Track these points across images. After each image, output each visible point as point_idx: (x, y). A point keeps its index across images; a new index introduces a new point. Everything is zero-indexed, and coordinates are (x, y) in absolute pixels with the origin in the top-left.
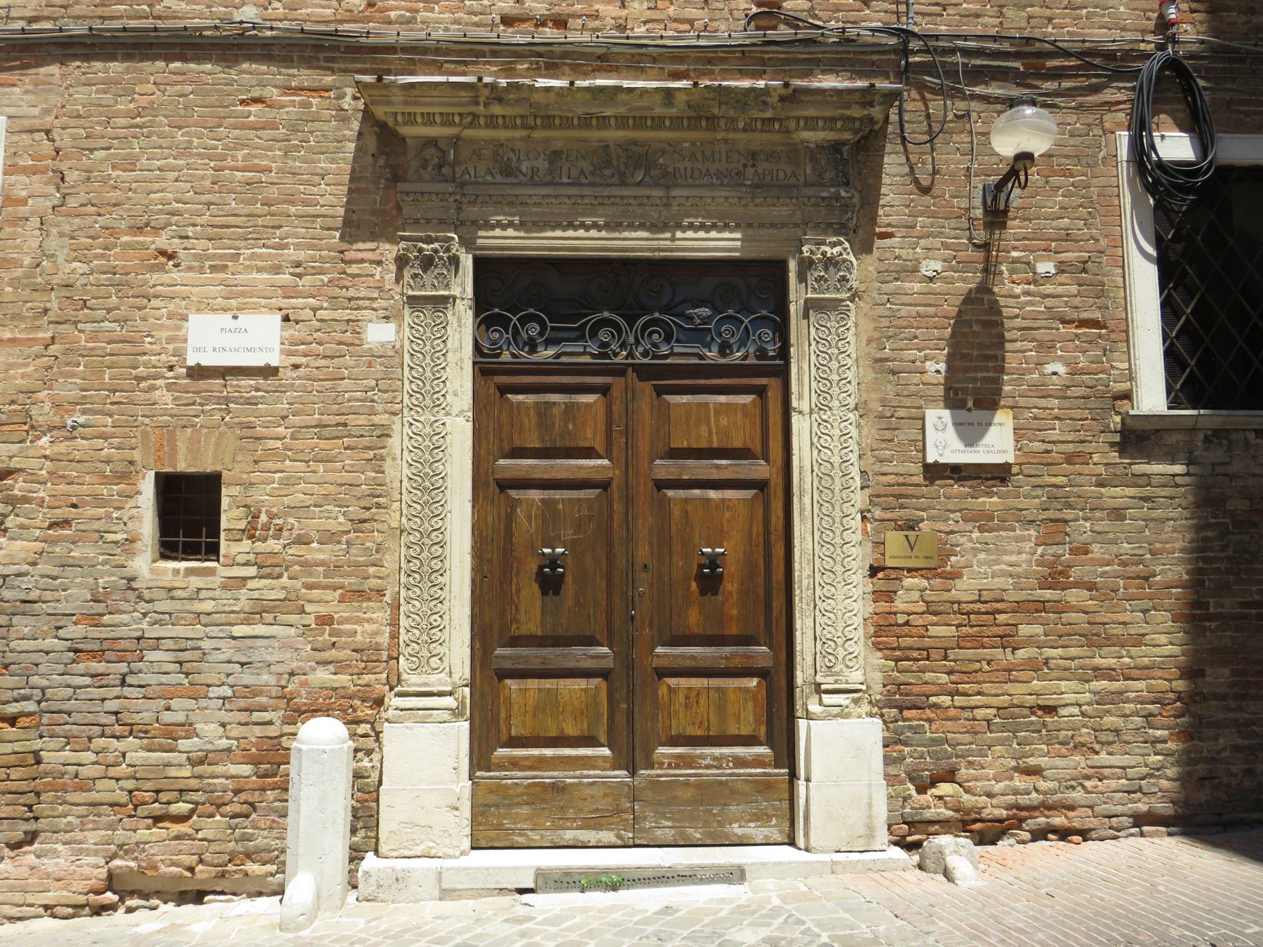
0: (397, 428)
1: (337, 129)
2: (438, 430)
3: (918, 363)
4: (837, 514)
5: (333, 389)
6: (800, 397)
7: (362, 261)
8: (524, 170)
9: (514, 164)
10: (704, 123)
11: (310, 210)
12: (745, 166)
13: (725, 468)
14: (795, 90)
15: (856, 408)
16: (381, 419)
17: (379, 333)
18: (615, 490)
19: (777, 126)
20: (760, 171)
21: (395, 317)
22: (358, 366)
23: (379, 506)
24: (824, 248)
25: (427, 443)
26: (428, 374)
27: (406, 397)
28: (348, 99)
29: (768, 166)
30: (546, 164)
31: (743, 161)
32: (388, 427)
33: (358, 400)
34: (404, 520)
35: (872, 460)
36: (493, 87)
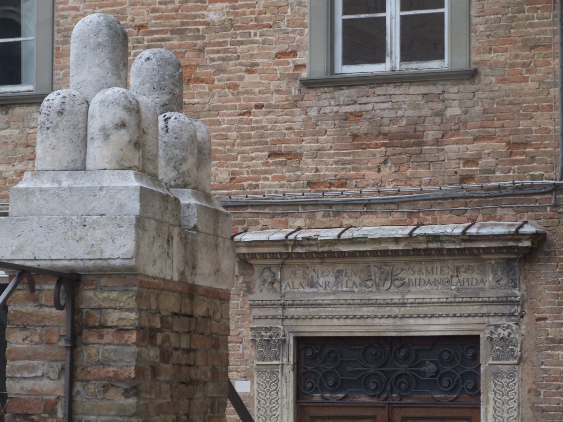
8: (321, 283)
9: (315, 280)
12: (452, 276)
26: (268, 413)
29: (466, 276)
31: (451, 273)
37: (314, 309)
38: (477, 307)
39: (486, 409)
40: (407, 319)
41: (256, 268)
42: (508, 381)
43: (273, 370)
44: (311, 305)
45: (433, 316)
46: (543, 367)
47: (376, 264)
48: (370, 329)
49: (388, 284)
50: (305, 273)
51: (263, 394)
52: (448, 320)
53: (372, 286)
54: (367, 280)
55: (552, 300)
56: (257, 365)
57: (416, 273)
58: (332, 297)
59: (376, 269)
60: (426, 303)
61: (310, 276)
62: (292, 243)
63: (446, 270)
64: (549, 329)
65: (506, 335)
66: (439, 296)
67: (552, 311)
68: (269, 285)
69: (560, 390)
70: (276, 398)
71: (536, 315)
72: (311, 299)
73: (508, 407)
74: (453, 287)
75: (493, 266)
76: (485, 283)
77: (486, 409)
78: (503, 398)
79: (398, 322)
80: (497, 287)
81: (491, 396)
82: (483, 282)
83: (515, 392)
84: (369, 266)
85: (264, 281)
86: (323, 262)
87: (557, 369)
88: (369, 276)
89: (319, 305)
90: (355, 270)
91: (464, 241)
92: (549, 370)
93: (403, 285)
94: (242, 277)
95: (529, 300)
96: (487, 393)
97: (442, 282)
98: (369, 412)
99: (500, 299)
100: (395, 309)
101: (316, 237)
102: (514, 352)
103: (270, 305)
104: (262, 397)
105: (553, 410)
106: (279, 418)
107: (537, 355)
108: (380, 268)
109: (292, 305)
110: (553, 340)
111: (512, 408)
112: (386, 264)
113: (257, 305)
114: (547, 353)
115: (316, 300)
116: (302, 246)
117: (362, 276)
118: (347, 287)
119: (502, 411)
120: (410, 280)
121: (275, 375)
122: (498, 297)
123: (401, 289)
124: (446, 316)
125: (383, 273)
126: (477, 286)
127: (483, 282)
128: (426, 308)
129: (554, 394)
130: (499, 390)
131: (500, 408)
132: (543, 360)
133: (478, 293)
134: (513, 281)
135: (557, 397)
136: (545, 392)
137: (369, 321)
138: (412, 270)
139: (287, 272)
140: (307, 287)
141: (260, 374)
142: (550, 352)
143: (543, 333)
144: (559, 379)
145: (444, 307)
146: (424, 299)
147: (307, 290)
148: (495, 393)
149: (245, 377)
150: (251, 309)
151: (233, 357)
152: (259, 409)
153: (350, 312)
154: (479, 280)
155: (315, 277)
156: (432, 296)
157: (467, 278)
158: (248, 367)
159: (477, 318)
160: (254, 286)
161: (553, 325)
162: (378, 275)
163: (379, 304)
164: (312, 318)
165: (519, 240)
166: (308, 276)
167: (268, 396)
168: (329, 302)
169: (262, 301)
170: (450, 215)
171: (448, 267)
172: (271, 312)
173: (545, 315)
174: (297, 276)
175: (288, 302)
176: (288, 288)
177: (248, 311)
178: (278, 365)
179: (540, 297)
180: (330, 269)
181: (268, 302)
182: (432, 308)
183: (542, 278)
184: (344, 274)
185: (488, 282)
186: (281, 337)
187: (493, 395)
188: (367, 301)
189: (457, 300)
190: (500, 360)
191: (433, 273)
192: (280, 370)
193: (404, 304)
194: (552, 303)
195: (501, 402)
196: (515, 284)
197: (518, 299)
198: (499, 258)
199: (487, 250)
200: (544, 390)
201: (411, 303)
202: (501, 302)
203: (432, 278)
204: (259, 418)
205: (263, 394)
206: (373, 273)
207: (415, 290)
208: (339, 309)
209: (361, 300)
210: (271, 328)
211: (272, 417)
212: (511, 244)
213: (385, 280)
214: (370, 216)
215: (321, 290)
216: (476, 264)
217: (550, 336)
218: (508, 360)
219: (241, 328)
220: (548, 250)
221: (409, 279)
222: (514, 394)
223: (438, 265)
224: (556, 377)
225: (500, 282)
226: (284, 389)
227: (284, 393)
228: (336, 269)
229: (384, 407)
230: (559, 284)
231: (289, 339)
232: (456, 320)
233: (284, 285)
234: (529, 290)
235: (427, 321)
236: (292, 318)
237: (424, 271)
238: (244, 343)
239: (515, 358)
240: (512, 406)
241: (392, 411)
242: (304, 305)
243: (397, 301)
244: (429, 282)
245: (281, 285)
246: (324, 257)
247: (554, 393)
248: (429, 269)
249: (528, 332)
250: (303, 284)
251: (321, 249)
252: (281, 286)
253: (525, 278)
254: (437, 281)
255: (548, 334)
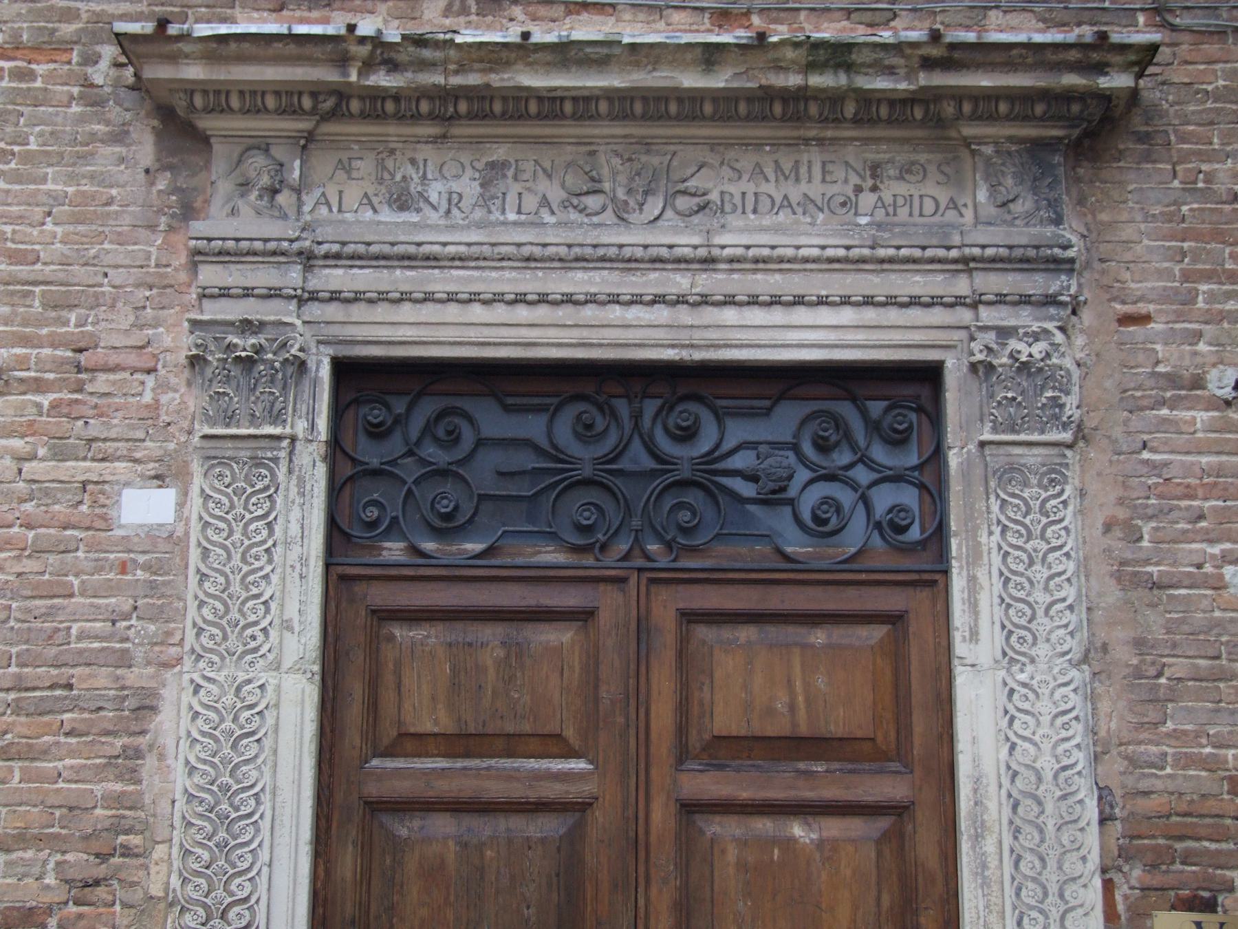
0: (168, 693)
1: (81, 119)
2: (251, 700)
3: (1208, 568)
4: (1052, 878)
5: (49, 614)
6: (974, 635)
7: (116, 368)
8: (434, 198)
9: (414, 187)
10: (778, 109)
11: (22, 270)
12: (858, 190)
13: (825, 781)
14: (953, 46)
15: (1085, 659)
16: (136, 676)
17: (145, 507)
18: (600, 818)
19: (918, 113)
20: (888, 198)
21: (176, 476)
22: (99, 570)
23: (127, 852)
24: (1013, 344)
25: (228, 724)
26: (236, 588)
27: (190, 634)
28: (104, 64)
29: (901, 188)
30: (476, 188)
31: (854, 180)
32: (154, 694)
33: (97, 638)
34: (175, 882)
35: (1121, 765)
36: (376, 41)
37: (409, 273)
38: (940, 277)
39: (972, 580)
40: (715, 310)
41: (218, 147)
42: (1044, 495)
43: (260, 454)
44: (403, 257)
45: (799, 301)
46: (1146, 455)
47: (615, 147)
48: (594, 336)
49: (654, 206)
50: (381, 165)
51: (218, 530)
52: (847, 315)
53: (604, 209)
54: (587, 193)
55: (1166, 265)
56: (205, 437)
57: (746, 177)
58: (474, 237)
59: (616, 161)
60: (781, 260)
61: (398, 178)
62: (364, 50)
63: (839, 173)
64: (1158, 347)
65: (1038, 356)
66: (822, 242)
67: (1165, 297)
68: (260, 197)
69: (1203, 524)
70: (264, 542)
71: (1118, 307)
72: (402, 238)
73: (1046, 573)
74: (863, 220)
75: (988, 161)
76: (963, 210)
77: (972, 580)
78: (1028, 546)
79: (684, 315)
80: (1005, 222)
81: (990, 541)
82: (956, 208)
83: (1066, 528)
84: (592, 153)
85: (245, 186)
86: (444, 136)
87: (1193, 464)
88: (593, 179)
89: (427, 258)
90: (547, 165)
91: (928, 64)
92: (1166, 464)
93: (702, 208)
94: (168, 174)
95: (1097, 266)
96: (973, 533)
97: (825, 206)
98: (570, 598)
99: (1018, 253)
100: (678, 277)
101: (448, 36)
102: (1062, 406)
103: (264, 253)
104: (215, 538)
105: (1186, 583)
106: (273, 605)
107: (1126, 422)
108: (630, 160)
109: (337, 256)
110: (1172, 380)
111: (1060, 574)
112: (646, 145)
113: (220, 253)
114: (1156, 416)
115: (419, 244)
116: (393, 66)
117: (569, 180)
118: (519, 212)
119: (1027, 585)
120: (727, 197)
121: (264, 472)
122: (1010, 247)
123: (696, 219)
124: (842, 303)
125: (638, 174)
126: (937, 219)
127: (956, 208)
128: (778, 277)
129: (1185, 537)
130: (1016, 522)
131: (1022, 575)
132: (1146, 437)
133: (946, 235)
134: (1049, 205)
135: (1194, 546)
136: (1156, 529)
137: (589, 312)
138: (733, 169)
139: (323, 163)
140: (386, 208)
141: (213, 466)
142: (1165, 412)
143: (1141, 357)
144: (1200, 493)
145: (836, 276)
146: (773, 247)
147: (387, 215)
148: (1005, 529)
149: (157, 477)
150: (193, 267)
151: (120, 414)
152: (203, 577)
153: (531, 282)
154: (943, 202)
155: (416, 180)
156: (803, 240)
157: (907, 194)
158: (172, 446)
159: (937, 310)
160: (207, 202)
161: (1169, 338)
162: (622, 179)
163: (629, 260)
164: (400, 300)
165: (1101, 68)
166: (393, 176)
167: (237, 536)
168: (462, 249)
169: (237, 240)
170: (845, 23)
171: (847, 163)
172: (263, 276)
173: (1143, 308)
174: (355, 174)
175: (324, 248)
176: (324, 210)
177: (183, 276)
178: (279, 438)
179: (1128, 256)
180: (465, 158)
181: (258, 245)
182: (796, 278)
183: (1131, 204)
184: (510, 173)
185: (979, 209)
186: (293, 351)
187: (996, 537)
188: (588, 251)
189: (882, 253)
190: (1018, 433)
191: (797, 180)
192: (283, 454)
193: (709, 262)
194: (1167, 274)
195: (1024, 557)
196: (1055, 212)
197: (1071, 253)
198: (1011, 139)
199: (985, 105)
200: (1154, 525)
201: (731, 261)
202: (1021, 261)
203: (795, 193)
204: (202, 604)
205: (218, 530)
206: (605, 171)
207: (741, 223)
208: (494, 274)
209: (570, 246)
210: (262, 324)
211: (250, 604)
212: (1071, 80)
213: (646, 193)
214: (596, 18)
215: (434, 217)
216: (931, 156)
217: (1161, 369)
218: (1042, 432)
219: (155, 327)
220: (1144, 129)
221: (722, 193)
222: (1063, 533)
223: (814, 156)
224: (1188, 486)
225: (1011, 206)
226: (295, 514)
227: (294, 529)
228: (484, 160)
229: (623, 580)
230: (1183, 220)
231: (319, 363)
232: (870, 315)
233: (309, 201)
234: (1094, 235)
235: (777, 316)
236: (334, 297)
237: (769, 171)
238: (162, 372)
239: (1065, 426)
240: (1060, 568)
241: (648, 594)
242: (377, 258)
243: (687, 251)
244: (786, 202)
245: (299, 199)
246: (456, 116)
247: (1185, 532)
248: (787, 166)
249: (1097, 355)
250: (375, 200)
251: (456, 80)
252: (300, 203)
253: (1081, 202)
254: (812, 201)
255: (1158, 362)
